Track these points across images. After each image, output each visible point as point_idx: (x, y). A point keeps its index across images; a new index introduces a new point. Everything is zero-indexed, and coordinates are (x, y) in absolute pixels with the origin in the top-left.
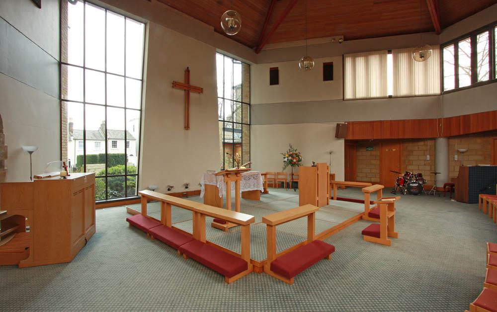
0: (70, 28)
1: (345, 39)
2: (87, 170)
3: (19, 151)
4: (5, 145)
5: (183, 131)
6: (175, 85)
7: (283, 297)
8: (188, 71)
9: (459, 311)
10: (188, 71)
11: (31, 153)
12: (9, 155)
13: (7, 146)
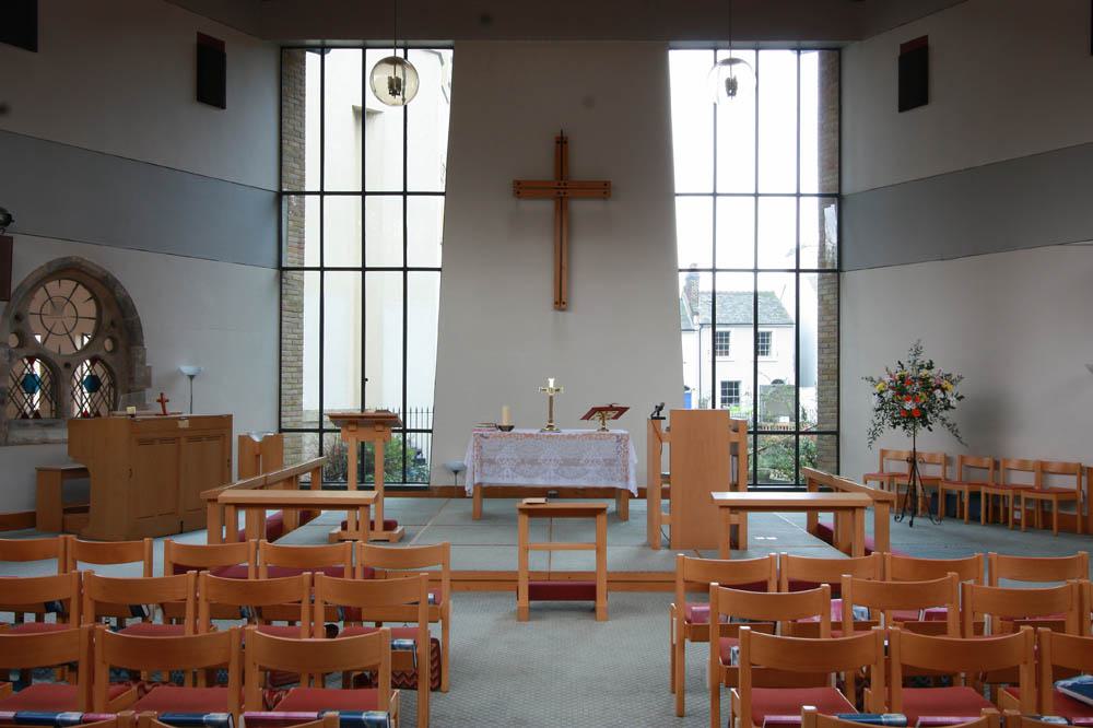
0: (354, 107)
2: (1076, 589)
4: (148, 364)
6: (523, 189)
8: (562, 142)
9: (85, 390)
10: (562, 142)
11: (192, 377)
12: (154, 382)
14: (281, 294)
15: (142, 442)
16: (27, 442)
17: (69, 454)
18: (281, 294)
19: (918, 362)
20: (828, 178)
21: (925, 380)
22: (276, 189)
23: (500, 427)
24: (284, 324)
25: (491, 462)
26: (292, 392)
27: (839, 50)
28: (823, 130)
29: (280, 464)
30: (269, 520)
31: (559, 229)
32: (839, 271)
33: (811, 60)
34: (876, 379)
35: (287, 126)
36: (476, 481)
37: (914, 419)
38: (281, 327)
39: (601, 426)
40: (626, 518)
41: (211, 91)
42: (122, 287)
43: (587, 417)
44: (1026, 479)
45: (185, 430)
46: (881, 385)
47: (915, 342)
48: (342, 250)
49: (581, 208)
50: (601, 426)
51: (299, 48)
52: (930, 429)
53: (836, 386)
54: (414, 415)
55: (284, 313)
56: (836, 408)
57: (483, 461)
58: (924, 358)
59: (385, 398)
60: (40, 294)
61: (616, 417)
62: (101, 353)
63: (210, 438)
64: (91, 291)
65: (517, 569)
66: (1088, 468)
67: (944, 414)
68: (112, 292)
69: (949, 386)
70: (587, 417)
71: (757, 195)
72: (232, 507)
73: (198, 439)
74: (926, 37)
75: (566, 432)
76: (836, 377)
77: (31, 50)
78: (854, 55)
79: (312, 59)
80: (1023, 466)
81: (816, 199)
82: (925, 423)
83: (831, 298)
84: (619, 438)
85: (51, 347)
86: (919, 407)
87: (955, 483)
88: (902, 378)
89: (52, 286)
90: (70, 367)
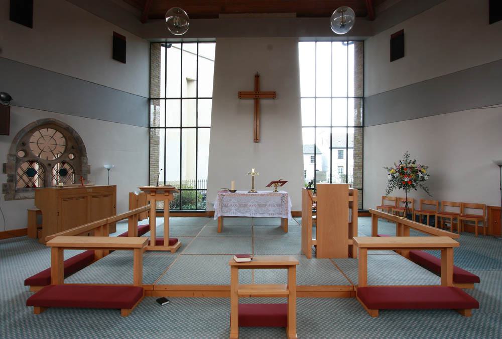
1: (298, 16)
3: (103, 169)
4: (88, 164)
5: (253, 144)
6: (242, 95)
7: (151, 330)
8: (257, 77)
10: (257, 77)
11: (109, 169)
12: (91, 172)
13: (90, 166)
14: (150, 137)
15: (66, 199)
16: (25, 198)
17: (35, 205)
18: (150, 137)
19: (408, 161)
20: (358, 91)
21: (411, 168)
22: (147, 96)
23: (230, 191)
24: (151, 149)
25: (226, 206)
26: (154, 175)
27: (363, 41)
28: (356, 73)
29: (115, 214)
30: (65, 261)
31: (256, 122)
32: (363, 127)
33: (352, 47)
34: (389, 168)
35: (153, 73)
36: (219, 216)
37: (405, 185)
38: (150, 150)
39: (275, 190)
40: (286, 232)
41: (119, 54)
42: (76, 132)
43: (269, 186)
44: (457, 210)
45: (90, 192)
46: (393, 170)
47: (406, 152)
48: (173, 121)
49: (264, 102)
50: (275, 190)
51: (157, 43)
52: (416, 189)
53: (362, 171)
54: (202, 182)
55: (151, 145)
56: (362, 180)
57: (223, 206)
58: (411, 158)
59: (188, 179)
60: (37, 134)
61: (281, 186)
62: (67, 160)
63: (104, 196)
64: (62, 134)
65: (229, 284)
66: (488, 206)
67: (421, 183)
68: (72, 133)
69: (424, 171)
70: (269, 186)
71: (332, 98)
72: (57, 249)
73: (98, 196)
74: (403, 30)
75: (260, 192)
76: (362, 168)
77: (29, 27)
78: (370, 43)
79: (163, 49)
80: (454, 205)
81: (353, 99)
82: (414, 187)
83: (360, 138)
84: (284, 196)
85: (43, 157)
86: (411, 180)
87: (418, 211)
88: (402, 168)
89: (44, 131)
90: (51, 165)
